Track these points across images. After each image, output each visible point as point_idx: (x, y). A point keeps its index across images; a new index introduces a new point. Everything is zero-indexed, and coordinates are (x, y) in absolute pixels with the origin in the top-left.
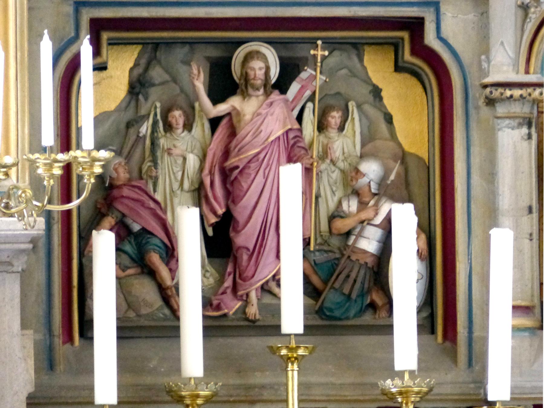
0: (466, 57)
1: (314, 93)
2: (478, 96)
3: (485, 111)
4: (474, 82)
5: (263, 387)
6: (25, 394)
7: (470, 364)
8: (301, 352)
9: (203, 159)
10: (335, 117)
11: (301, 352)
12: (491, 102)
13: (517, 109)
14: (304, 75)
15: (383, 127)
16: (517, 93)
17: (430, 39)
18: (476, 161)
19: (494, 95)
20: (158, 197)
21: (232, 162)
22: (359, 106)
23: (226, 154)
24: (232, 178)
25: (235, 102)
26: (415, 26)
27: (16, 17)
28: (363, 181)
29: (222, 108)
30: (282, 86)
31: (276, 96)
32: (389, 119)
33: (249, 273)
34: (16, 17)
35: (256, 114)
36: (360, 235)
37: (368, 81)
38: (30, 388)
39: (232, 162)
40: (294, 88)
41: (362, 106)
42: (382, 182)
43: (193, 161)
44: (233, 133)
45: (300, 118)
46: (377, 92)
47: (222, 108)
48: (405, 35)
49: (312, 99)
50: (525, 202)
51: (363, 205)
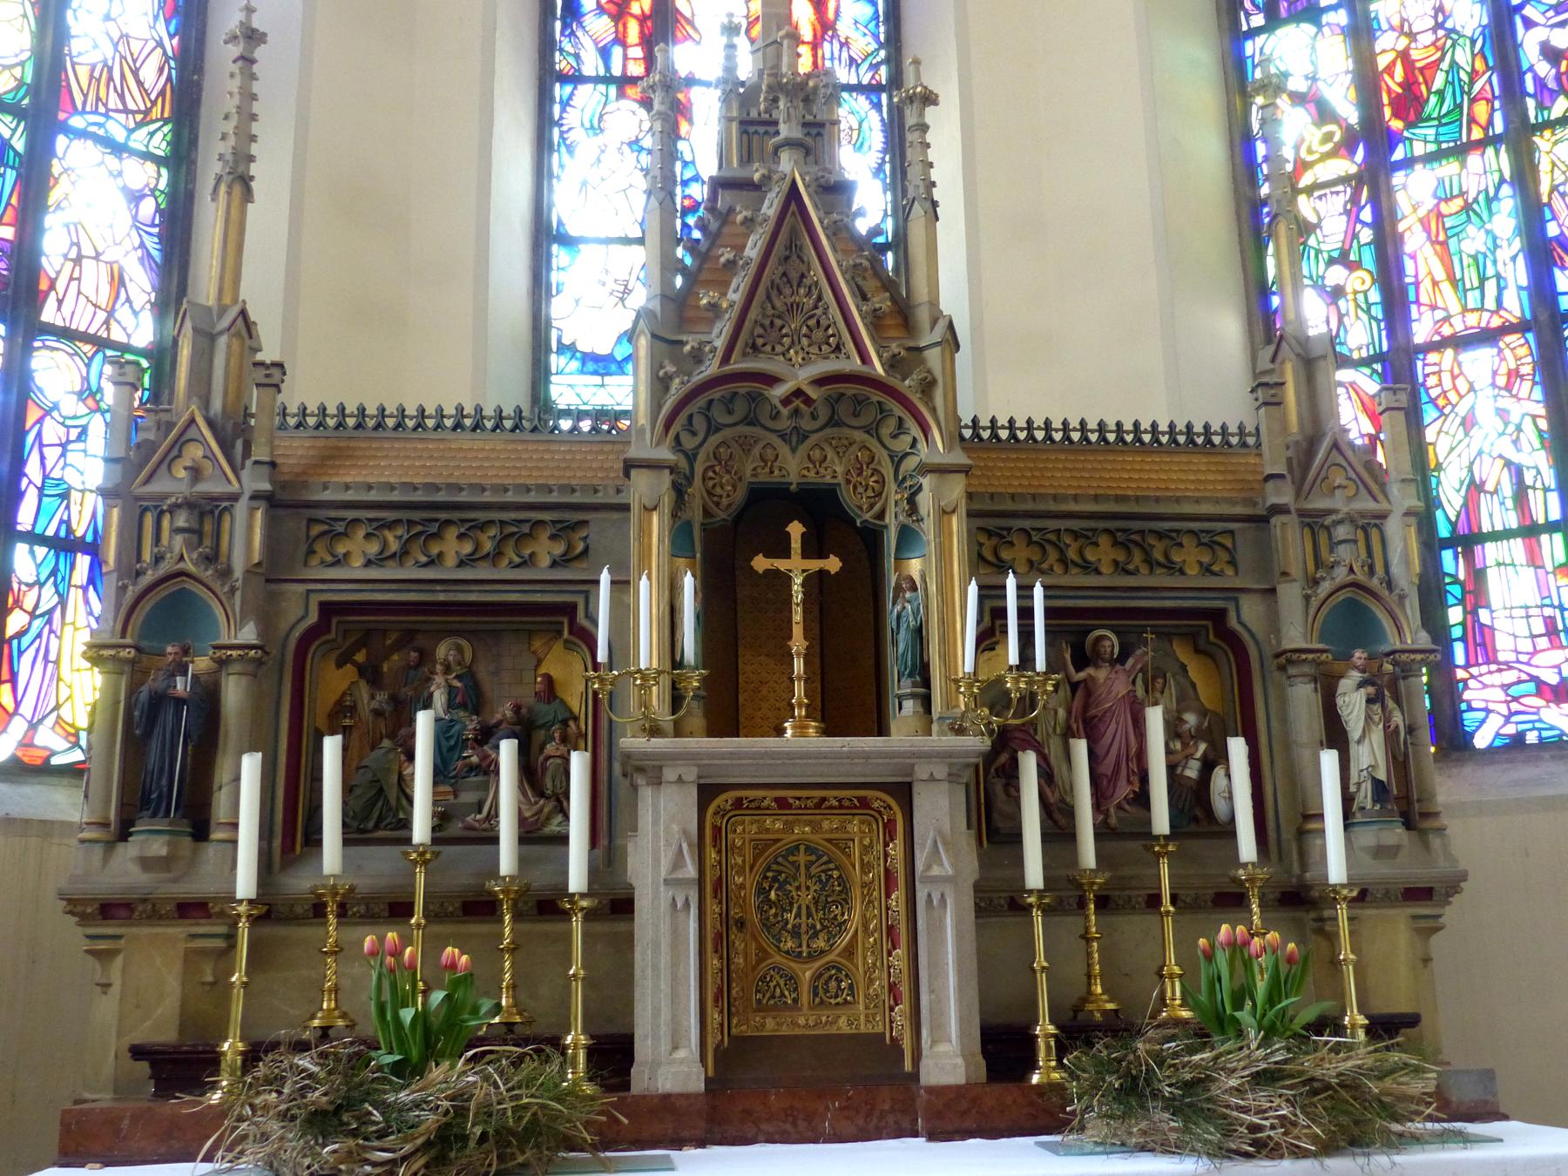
0: (1260, 636)
1: (779, 840)
2: (1272, 664)
3: (1276, 674)
4: (1268, 653)
5: (1132, 877)
6: (971, 882)
7: (1280, 859)
8: (1170, 848)
9: (1069, 712)
10: (1159, 685)
11: (1170, 848)
12: (1282, 668)
13: (1307, 669)
14: (1139, 652)
15: (1191, 691)
16: (1311, 656)
17: (1233, 622)
18: (1273, 711)
19: (1287, 660)
20: (1038, 738)
21: (1092, 712)
22: (1174, 676)
23: (1086, 707)
24: (1461, 560)
25: (1090, 671)
26: (1218, 616)
27: (610, 826)
28: (1187, 726)
29: (1082, 675)
30: (1122, 658)
31: (1118, 667)
32: (1194, 685)
33: (1109, 792)
34: (610, 826)
35: (1108, 678)
36: (1184, 767)
37: (1177, 660)
38: (976, 876)
39: (1092, 712)
40: (1130, 662)
41: (1478, 549)
42: (1198, 728)
43: (1062, 713)
44: (1089, 694)
45: (1134, 682)
46: (1184, 668)
47: (1082, 675)
48: (1209, 624)
49: (1141, 670)
50: (1317, 737)
51: (1185, 745)
